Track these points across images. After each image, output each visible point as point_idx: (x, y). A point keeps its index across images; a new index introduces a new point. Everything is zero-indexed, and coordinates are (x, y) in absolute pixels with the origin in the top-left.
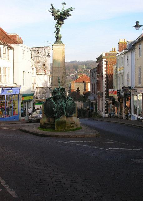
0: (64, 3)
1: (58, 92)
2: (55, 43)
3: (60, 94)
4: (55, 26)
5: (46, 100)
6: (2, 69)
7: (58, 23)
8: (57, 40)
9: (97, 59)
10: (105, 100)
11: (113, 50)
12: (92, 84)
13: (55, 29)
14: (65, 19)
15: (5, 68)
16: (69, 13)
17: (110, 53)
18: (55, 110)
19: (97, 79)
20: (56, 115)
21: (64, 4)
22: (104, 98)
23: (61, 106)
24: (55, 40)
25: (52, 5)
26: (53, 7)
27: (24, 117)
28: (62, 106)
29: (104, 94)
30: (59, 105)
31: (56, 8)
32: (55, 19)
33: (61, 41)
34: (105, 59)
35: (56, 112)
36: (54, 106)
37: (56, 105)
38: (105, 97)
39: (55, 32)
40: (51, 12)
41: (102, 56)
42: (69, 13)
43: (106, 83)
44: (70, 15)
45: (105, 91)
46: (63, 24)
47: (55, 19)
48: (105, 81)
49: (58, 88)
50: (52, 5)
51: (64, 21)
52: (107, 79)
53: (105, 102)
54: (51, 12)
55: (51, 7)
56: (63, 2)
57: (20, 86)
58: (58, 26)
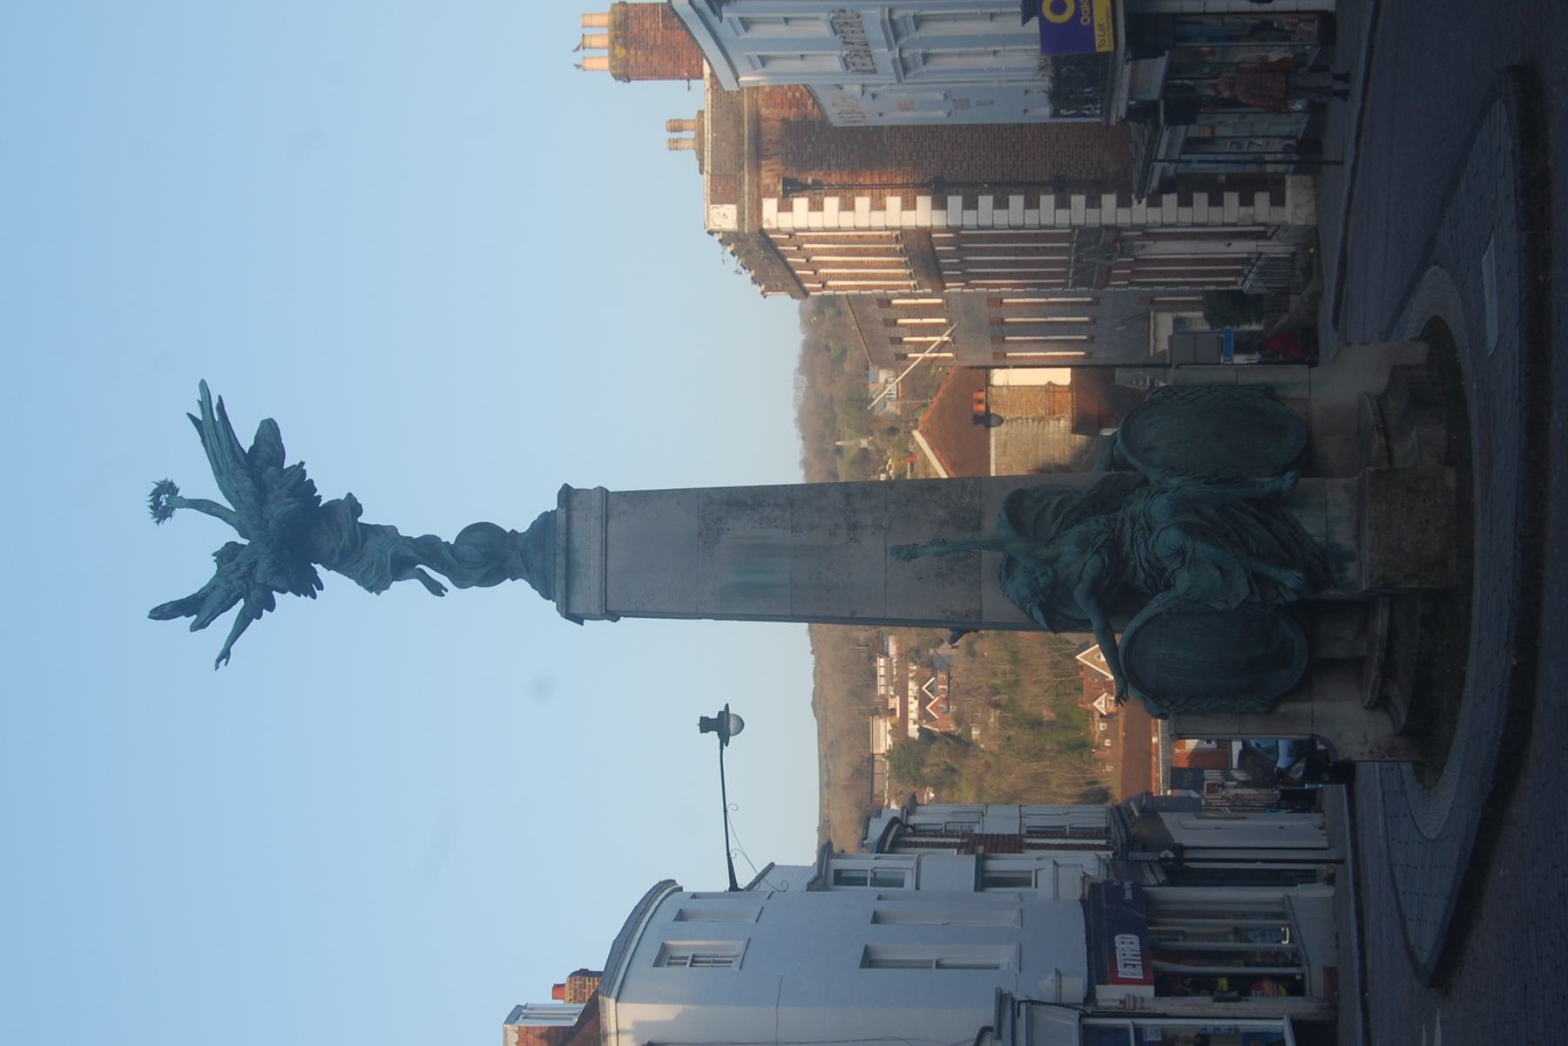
0: (156, 495)
1: (1051, 562)
3: (1067, 549)
13: (407, 590)
16: (246, 441)
17: (707, 168)
18: (1242, 586)
21: (165, 501)
22: (1140, 213)
25: (162, 613)
30: (1181, 553)
31: (199, 574)
34: (770, 206)
35: (1256, 578)
37: (1183, 580)
38: (1124, 203)
39: (437, 589)
41: (727, 238)
42: (246, 441)
43: (1017, 201)
44: (269, 433)
45: (1185, 201)
47: (307, 586)
48: (1002, 204)
49: (1000, 555)
50: (162, 613)
51: (328, 491)
52: (1078, 187)
53: (1170, 200)
55: (185, 622)
56: (147, 512)
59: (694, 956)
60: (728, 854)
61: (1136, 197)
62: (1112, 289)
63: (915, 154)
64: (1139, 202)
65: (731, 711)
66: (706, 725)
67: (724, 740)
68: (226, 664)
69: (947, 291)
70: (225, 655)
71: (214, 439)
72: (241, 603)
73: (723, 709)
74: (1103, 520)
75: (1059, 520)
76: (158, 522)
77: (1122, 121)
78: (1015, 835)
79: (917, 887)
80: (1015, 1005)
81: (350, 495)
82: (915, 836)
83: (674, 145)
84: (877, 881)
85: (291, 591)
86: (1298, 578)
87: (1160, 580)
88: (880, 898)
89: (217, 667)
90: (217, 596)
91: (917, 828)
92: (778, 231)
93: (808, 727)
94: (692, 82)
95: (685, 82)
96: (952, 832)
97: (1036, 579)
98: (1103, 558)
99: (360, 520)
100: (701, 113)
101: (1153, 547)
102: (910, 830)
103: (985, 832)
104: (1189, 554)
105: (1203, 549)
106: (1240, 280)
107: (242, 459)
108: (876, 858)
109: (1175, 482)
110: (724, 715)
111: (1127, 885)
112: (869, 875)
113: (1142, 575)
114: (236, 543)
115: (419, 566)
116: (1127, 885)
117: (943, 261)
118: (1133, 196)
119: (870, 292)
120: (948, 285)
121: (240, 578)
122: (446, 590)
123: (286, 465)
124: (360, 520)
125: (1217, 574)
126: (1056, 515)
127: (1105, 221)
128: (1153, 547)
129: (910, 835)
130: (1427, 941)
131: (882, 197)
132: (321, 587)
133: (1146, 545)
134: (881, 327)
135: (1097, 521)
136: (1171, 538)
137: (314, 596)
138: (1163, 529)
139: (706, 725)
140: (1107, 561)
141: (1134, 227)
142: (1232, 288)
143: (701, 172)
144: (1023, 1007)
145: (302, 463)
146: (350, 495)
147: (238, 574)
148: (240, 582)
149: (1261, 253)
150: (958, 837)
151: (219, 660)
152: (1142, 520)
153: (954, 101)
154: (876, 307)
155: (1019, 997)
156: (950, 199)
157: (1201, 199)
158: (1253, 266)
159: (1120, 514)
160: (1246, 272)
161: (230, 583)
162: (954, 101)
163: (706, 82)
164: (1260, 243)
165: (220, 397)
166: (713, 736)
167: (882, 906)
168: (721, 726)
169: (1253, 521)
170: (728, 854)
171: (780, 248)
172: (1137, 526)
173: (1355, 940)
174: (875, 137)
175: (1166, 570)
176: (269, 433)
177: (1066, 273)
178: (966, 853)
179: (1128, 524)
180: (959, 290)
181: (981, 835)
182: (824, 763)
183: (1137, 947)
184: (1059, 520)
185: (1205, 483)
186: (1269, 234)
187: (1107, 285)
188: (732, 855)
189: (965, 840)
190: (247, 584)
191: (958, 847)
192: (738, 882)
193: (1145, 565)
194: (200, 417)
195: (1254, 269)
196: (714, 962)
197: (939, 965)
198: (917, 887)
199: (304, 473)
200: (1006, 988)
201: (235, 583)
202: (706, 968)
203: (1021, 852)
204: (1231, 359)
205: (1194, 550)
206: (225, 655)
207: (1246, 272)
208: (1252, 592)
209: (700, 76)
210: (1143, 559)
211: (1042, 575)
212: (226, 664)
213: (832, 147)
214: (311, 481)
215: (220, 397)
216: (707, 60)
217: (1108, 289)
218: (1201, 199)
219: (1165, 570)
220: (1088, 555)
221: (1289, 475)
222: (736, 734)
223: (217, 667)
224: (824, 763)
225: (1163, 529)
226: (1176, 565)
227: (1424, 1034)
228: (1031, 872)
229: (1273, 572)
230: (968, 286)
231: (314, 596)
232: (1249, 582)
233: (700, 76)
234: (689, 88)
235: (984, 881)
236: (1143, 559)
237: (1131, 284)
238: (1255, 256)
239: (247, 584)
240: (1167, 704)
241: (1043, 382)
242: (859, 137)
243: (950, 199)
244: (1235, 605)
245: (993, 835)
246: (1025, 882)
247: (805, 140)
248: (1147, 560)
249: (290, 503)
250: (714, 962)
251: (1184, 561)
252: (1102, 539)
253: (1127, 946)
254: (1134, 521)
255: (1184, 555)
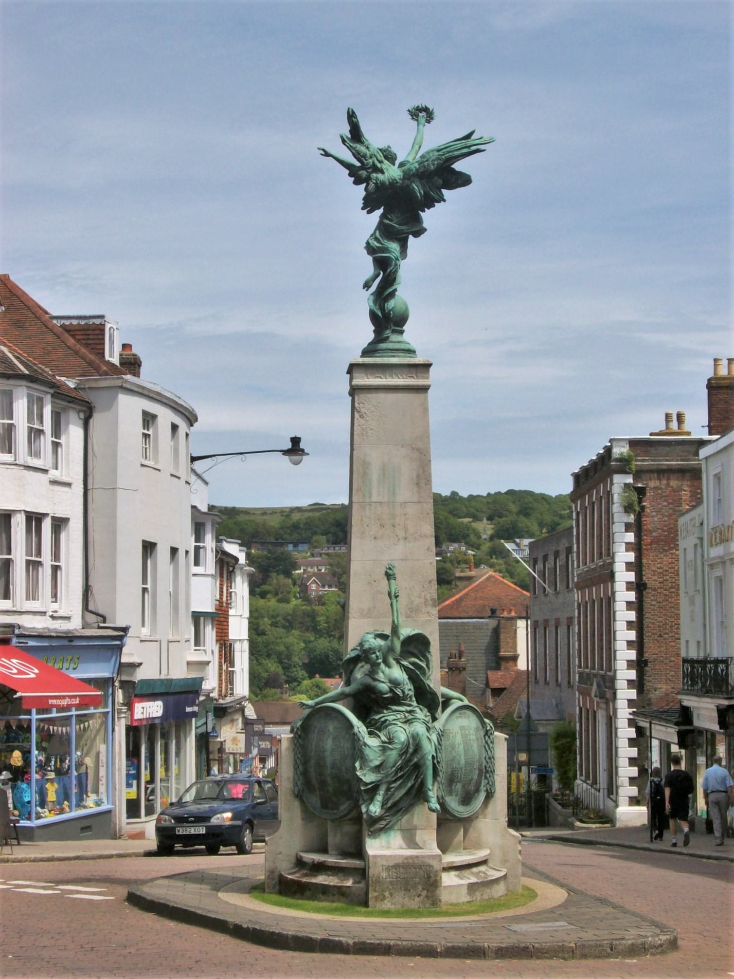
0: (426, 110)
2: (366, 353)
3: (397, 673)
4: (370, 250)
5: (307, 711)
6: (19, 525)
7: (385, 230)
8: (380, 337)
9: (577, 477)
10: (632, 723)
11: (674, 425)
12: (540, 631)
13: (367, 267)
14: (430, 201)
15: (34, 520)
18: (369, 777)
19: (577, 596)
20: (375, 809)
22: (624, 712)
23: (404, 752)
24: (366, 333)
25: (351, 116)
26: (356, 134)
27: (143, 818)
28: (415, 746)
29: (621, 685)
30: (391, 741)
32: (369, 204)
33: (405, 337)
35: (374, 789)
36: (357, 750)
37: (373, 742)
39: (367, 285)
40: (341, 162)
41: (608, 450)
42: (458, 166)
44: (463, 180)
46: (417, 234)
47: (369, 204)
49: (388, 631)
50: (351, 116)
51: (428, 217)
53: (632, 733)
54: (341, 162)
55: (346, 130)
57: (125, 630)
58: (385, 250)
59: (149, 435)
60: (214, 456)
61: (634, 712)
62: (577, 696)
63: (661, 570)
64: (630, 714)
65: (304, 457)
66: (295, 441)
67: (286, 452)
68: (321, 154)
69: (575, 590)
70: (327, 154)
71: (459, 146)
72: (358, 164)
73: (306, 451)
74: (412, 693)
75: (411, 667)
76: (409, 111)
77: (680, 701)
78: (228, 636)
79: (194, 575)
80: (120, 638)
81: (425, 230)
82: (227, 573)
83: (668, 417)
84: (197, 549)
85: (366, 195)
86: (375, 812)
87: (375, 728)
88: (187, 552)
89: (319, 149)
90: (361, 148)
91: (233, 574)
92: (612, 484)
93: (304, 502)
94: (707, 428)
95: (707, 424)
96: (231, 596)
97: (375, 653)
98: (386, 694)
99: (411, 237)
100: (689, 434)
101: (394, 724)
102: (231, 569)
103: (230, 618)
104: (390, 746)
105: (393, 755)
106: (583, 778)
107: (448, 164)
108: (212, 549)
109: (434, 737)
110: (302, 452)
111: (196, 709)
112: (201, 544)
113: (377, 717)
114: (396, 159)
115: (382, 273)
116: (196, 709)
117: (587, 590)
118: (635, 710)
119: (575, 542)
120: (580, 592)
121: (373, 163)
122: (367, 290)
123: (444, 191)
124: (411, 237)
125: (377, 763)
126: (413, 664)
127: (619, 692)
128: (394, 724)
129: (228, 570)
130: (150, 892)
131: (633, 550)
132: (369, 212)
133: (395, 720)
134: (554, 548)
135: (410, 690)
136: (401, 734)
137: (363, 209)
138: (405, 730)
139: (295, 441)
140: (386, 696)
141: (615, 710)
142: (578, 773)
143: (651, 434)
144: (118, 643)
145: (444, 201)
146: (425, 230)
147: (376, 162)
148: (371, 163)
149: (599, 791)
150: (227, 600)
151: (324, 150)
152: (411, 717)
153: (694, 596)
154: (567, 545)
155: (125, 639)
156: (633, 593)
157: (634, 752)
158: (592, 786)
159: (415, 704)
160: (588, 782)
161: (371, 157)
162: (694, 596)
163: (706, 437)
164: (606, 791)
165: (484, 150)
166: (289, 445)
167: (181, 554)
168: (295, 449)
169: (409, 785)
170: (214, 456)
171: (602, 485)
172: (407, 714)
173: (698, 853)
174: (672, 545)
175: (380, 731)
176: (463, 180)
177: (587, 668)
178: (216, 605)
179: (408, 708)
180: (576, 599)
181: (228, 615)
182: (278, 511)
183: (155, 715)
184: (411, 667)
185: (433, 756)
186: (611, 796)
187: (580, 693)
188: (213, 458)
189: (224, 605)
190: (369, 168)
191: (220, 601)
192: (197, 462)
193: (383, 719)
194: (473, 137)
195: (589, 787)
196: (146, 448)
197: (145, 590)
198: (194, 575)
199: (439, 202)
200: (131, 633)
201: (370, 160)
202: (186, 400)
203: (217, 641)
204: (535, 772)
205: (392, 749)
206: (327, 154)
207: (588, 782)
208: (366, 784)
209: (710, 434)
210: (386, 718)
211: (377, 657)
212: (321, 154)
213: (666, 518)
214: (434, 206)
215: (484, 150)
216: (720, 438)
217: (577, 693)
218: (634, 752)
219: (380, 731)
220: (389, 685)
221: (438, 807)
222: (291, 461)
223: (319, 149)
224: (278, 511)
225: (405, 730)
226: (384, 738)
227: (99, 890)
228: (204, 646)
229: (379, 798)
230: (579, 605)
231: (363, 209)
232: (372, 783)
233: (710, 434)
234: (703, 427)
235: (197, 617)
236: (386, 718)
237: (581, 709)
238: (598, 787)
239: (369, 168)
240: (299, 733)
241: (519, 652)
242: (672, 535)
243: (633, 593)
244: (358, 773)
245: (228, 622)
246: (197, 642)
247: (671, 501)
248: (386, 720)
249: (420, 193)
250: (146, 448)
251: (385, 742)
252: (399, 692)
253: (153, 709)
254: (410, 712)
255: (390, 743)
